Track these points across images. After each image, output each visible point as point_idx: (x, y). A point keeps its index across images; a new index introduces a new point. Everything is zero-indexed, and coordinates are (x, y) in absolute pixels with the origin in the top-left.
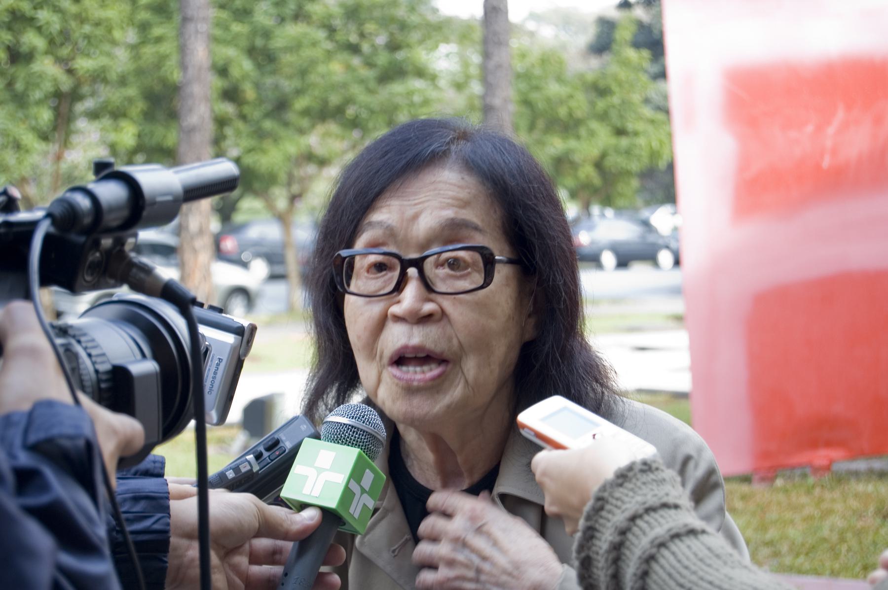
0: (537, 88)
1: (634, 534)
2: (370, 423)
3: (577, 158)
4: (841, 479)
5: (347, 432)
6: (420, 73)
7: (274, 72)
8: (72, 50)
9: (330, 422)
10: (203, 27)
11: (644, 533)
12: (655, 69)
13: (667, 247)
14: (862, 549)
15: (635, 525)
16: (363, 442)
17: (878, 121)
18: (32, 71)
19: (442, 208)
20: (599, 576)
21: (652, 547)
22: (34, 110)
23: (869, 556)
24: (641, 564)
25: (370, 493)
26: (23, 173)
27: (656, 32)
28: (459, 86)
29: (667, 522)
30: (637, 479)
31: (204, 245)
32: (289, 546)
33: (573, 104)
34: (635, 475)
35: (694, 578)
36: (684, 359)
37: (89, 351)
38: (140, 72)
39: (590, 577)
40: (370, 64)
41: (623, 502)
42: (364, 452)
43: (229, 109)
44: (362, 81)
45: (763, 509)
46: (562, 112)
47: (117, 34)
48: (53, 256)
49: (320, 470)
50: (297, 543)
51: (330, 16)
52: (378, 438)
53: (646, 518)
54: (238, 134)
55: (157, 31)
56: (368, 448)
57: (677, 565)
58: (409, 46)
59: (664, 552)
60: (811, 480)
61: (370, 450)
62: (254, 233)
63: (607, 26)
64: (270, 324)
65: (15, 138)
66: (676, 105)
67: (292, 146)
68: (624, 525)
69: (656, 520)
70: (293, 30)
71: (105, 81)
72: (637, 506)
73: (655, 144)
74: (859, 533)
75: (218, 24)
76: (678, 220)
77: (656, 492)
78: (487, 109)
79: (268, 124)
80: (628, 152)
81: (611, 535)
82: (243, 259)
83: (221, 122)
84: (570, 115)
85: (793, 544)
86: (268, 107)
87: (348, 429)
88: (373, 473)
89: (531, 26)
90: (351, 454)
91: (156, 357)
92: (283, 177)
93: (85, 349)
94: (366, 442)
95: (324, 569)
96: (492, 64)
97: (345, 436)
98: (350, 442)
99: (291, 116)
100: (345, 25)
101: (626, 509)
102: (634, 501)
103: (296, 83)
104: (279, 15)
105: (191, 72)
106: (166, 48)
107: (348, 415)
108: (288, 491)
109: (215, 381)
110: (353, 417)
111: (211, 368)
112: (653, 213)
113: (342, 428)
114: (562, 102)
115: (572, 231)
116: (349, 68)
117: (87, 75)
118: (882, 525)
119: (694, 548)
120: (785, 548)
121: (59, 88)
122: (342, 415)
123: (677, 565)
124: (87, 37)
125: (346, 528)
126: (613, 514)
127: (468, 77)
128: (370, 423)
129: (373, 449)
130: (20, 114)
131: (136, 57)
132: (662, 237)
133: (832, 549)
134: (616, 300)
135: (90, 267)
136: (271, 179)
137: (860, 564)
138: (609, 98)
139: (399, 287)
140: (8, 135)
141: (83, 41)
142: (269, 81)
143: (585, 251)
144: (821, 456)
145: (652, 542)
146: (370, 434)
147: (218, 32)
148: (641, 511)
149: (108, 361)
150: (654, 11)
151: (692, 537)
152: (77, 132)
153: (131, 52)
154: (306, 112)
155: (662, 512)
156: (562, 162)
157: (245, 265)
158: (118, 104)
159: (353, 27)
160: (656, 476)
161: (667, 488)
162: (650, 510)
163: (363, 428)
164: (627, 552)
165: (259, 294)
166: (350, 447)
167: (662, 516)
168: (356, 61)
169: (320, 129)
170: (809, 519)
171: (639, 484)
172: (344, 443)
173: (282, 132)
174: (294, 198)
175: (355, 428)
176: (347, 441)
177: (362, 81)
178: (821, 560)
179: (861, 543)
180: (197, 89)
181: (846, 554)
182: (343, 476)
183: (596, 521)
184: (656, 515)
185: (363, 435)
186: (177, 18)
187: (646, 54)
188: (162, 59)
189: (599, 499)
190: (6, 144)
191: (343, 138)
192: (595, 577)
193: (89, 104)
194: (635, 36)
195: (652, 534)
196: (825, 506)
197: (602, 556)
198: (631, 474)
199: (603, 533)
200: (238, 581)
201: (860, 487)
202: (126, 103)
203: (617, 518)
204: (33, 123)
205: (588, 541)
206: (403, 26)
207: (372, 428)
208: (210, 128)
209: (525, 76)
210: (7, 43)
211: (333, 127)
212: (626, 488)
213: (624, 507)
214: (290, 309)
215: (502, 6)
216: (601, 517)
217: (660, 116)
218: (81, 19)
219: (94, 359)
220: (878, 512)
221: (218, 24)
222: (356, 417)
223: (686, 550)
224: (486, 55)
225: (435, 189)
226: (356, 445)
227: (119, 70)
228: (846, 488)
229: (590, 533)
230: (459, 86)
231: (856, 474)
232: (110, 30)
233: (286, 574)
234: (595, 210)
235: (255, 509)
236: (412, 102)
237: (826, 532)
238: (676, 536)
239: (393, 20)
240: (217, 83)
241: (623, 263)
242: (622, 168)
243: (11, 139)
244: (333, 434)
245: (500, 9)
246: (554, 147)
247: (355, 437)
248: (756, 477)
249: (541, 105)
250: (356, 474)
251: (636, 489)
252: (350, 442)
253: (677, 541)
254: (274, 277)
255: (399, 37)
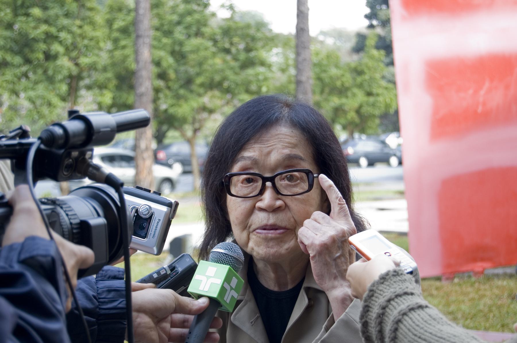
0: (325, 71)
1: (390, 309)
2: (235, 252)
3: (346, 108)
4: (489, 278)
5: (223, 257)
6: (263, 63)
7: (185, 64)
8: (78, 53)
9: (214, 252)
10: (147, 40)
11: (395, 308)
12: (387, 60)
13: (395, 155)
14: (501, 316)
15: (390, 304)
16: (232, 262)
17: (507, 87)
18: (57, 65)
19: (283, 149)
20: (372, 331)
21: (399, 315)
22: (58, 85)
23: (505, 320)
24: (393, 324)
25: (235, 290)
26: (53, 119)
27: (388, 40)
28: (283, 71)
29: (407, 302)
30: (391, 280)
31: (148, 156)
32: (192, 318)
33: (344, 79)
34: (390, 277)
35: (422, 331)
36: (404, 215)
37: (67, 212)
38: (114, 65)
39: (367, 332)
40: (236, 59)
41: (384, 292)
42: (232, 268)
43: (161, 83)
44: (232, 68)
45: (448, 295)
46: (338, 83)
47: (102, 44)
48: (46, 161)
49: (208, 277)
50: (196, 316)
51: (215, 34)
52: (240, 261)
53: (396, 300)
54: (166, 96)
55: (123, 43)
56: (234, 266)
57: (413, 324)
58: (256, 49)
59: (406, 317)
60: (473, 279)
61: (235, 267)
62: (174, 149)
63: (361, 38)
64: (183, 197)
65: (48, 100)
66: (399, 79)
67: (195, 103)
68: (384, 304)
69: (401, 301)
70: (195, 42)
71: (96, 69)
72: (391, 294)
73: (388, 100)
74: (499, 307)
75: (155, 39)
76: (401, 141)
77: (401, 286)
78: (298, 83)
79: (182, 92)
80: (373, 105)
81: (378, 309)
82: (169, 163)
83: (157, 91)
84: (343, 85)
85: (464, 313)
86: (182, 82)
87: (224, 255)
88: (237, 279)
89: (321, 38)
90: (225, 269)
91: (106, 217)
92: (190, 119)
93: (65, 211)
94: (233, 262)
95: (211, 330)
96: (300, 59)
97: (222, 259)
98: (224, 262)
99: (194, 87)
100: (223, 38)
101: (385, 296)
102: (389, 291)
103: (197, 70)
104: (187, 34)
105: (141, 64)
106: (128, 51)
107: (223, 248)
108: (191, 289)
109: (156, 231)
110: (226, 249)
111: (154, 224)
112: (387, 137)
113: (220, 255)
114: (338, 78)
115: (343, 147)
116: (225, 61)
117: (86, 66)
118: (511, 303)
119: (422, 315)
120: (459, 316)
121: (71, 73)
122: (221, 248)
123: (413, 324)
124: (86, 47)
125: (223, 309)
126: (379, 299)
127: (288, 66)
128: (235, 252)
129: (237, 266)
130: (51, 87)
131: (112, 57)
132: (392, 150)
133: (485, 316)
134: (368, 183)
135: (66, 167)
136: (184, 121)
137: (500, 324)
138: (363, 76)
139: (262, 192)
140: (44, 99)
141: (84, 48)
142: (182, 68)
143: (351, 157)
144: (478, 266)
145: (399, 313)
146: (235, 258)
147: (155, 43)
148: (393, 297)
149: (78, 218)
150: (387, 29)
151: (421, 310)
152: (81, 96)
153: (109, 54)
154: (202, 85)
155: (404, 297)
156: (338, 111)
157: (170, 166)
158: (102, 82)
159: (226, 40)
160: (401, 278)
161: (407, 284)
162: (398, 296)
163: (232, 255)
164: (386, 319)
165: (178, 181)
166: (224, 265)
167: (404, 299)
168: (229, 58)
169: (210, 94)
170: (473, 299)
171: (392, 282)
172: (221, 263)
173: (189, 95)
174: (196, 131)
175: (227, 255)
176: (223, 262)
177: (232, 68)
178: (479, 322)
179: (500, 312)
180: (144, 73)
181: (492, 318)
182: (221, 280)
183: (370, 302)
184: (401, 299)
185: (231, 259)
186: (133, 36)
187: (383, 52)
188: (126, 57)
189: (371, 291)
190: (43, 103)
191: (222, 99)
192: (370, 332)
193: (87, 81)
194: (377, 43)
195: (399, 309)
196: (481, 293)
197: (373, 321)
198: (387, 277)
199: (374, 309)
200: (164, 336)
201: (500, 283)
202: (107, 81)
203: (381, 300)
204: (58, 92)
205: (366, 313)
206: (253, 39)
207: (236, 255)
208: (151, 94)
209: (318, 65)
210: (43, 49)
211: (217, 93)
212: (385, 285)
213: (384, 295)
214: (194, 189)
215: (305, 28)
216: (372, 300)
217: (391, 86)
218: (83, 37)
219: (70, 217)
220: (509, 296)
221: (155, 39)
222: (228, 249)
223: (417, 317)
224: (298, 54)
225: (278, 138)
226: (228, 264)
227: (103, 63)
228: (492, 283)
229: (366, 309)
230: (283, 71)
231: (497, 276)
232: (98, 42)
233: (190, 333)
234: (356, 135)
235: (173, 297)
236: (258, 79)
237: (481, 307)
238: (412, 309)
239: (248, 35)
240: (155, 70)
241: (371, 163)
242: (370, 113)
243: (46, 100)
244: (216, 258)
245: (305, 29)
246: (334, 102)
247: (227, 260)
248: (444, 278)
249: (327, 80)
250: (228, 279)
251: (391, 285)
252: (224, 262)
253: (412, 312)
254: (185, 173)
255: (251, 45)
